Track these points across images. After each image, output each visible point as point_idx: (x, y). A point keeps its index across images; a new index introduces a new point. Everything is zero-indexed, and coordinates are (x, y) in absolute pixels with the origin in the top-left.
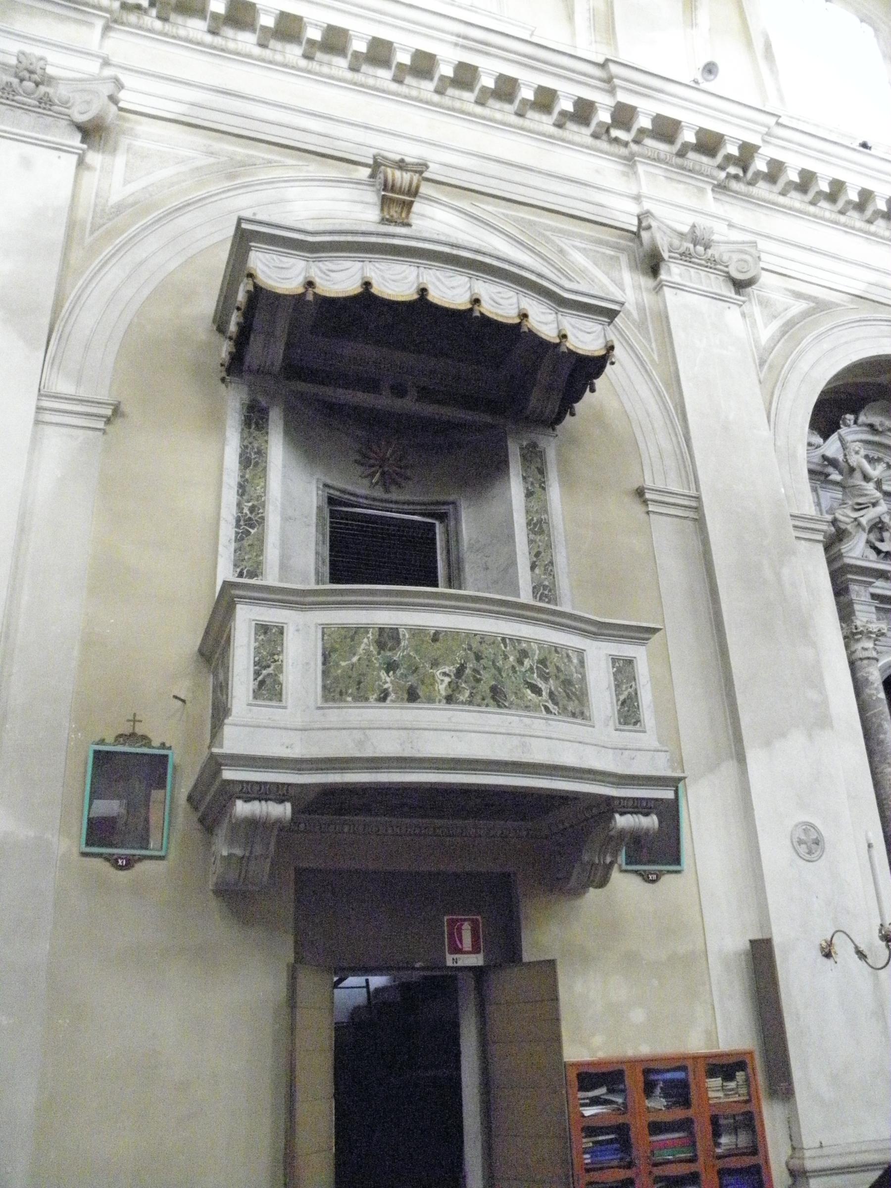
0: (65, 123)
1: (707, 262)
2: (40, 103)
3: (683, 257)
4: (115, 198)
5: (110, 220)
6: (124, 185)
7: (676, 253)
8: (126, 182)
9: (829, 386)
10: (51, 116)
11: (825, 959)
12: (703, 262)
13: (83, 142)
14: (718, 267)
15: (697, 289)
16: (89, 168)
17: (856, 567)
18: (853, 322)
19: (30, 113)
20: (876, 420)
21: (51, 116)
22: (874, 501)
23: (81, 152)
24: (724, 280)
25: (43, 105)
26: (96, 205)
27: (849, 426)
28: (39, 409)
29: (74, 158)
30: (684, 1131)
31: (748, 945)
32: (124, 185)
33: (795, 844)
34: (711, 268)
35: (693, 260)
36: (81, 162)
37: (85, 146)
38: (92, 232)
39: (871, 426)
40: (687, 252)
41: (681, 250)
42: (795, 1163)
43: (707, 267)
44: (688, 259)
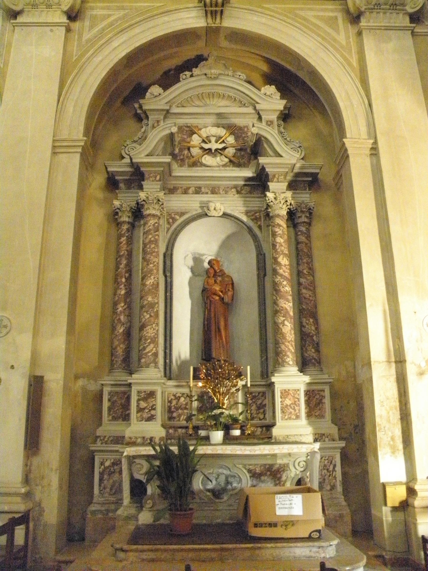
23: (66, 24)
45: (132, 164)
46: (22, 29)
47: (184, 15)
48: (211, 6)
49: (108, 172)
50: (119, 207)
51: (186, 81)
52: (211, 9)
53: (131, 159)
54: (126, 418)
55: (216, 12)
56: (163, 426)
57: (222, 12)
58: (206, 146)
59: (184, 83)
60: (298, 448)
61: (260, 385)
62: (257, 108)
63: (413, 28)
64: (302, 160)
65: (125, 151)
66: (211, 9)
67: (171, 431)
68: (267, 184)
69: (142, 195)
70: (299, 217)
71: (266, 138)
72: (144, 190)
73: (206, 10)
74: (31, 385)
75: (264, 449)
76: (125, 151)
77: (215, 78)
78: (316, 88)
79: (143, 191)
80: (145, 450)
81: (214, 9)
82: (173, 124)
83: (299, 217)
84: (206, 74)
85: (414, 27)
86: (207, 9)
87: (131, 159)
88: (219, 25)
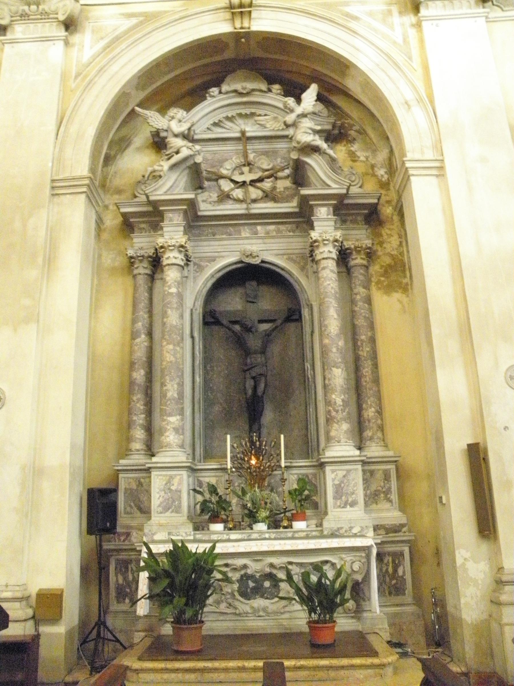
1: (41, 16)
3: (23, 18)
7: (16, 16)
12: (39, 17)
14: (51, 16)
15: (30, 38)
16: (73, 45)
17: (164, 201)
18: (172, 22)
20: (238, 86)
22: (175, 150)
23: (64, 38)
24: (57, 25)
27: (213, 97)
28: (53, 188)
29: (62, 43)
31: (466, 447)
34: (45, 19)
35: (31, 17)
36: (67, 43)
37: (67, 33)
39: (235, 91)
40: (24, 13)
41: (20, 12)
43: (41, 19)
44: (27, 18)
45: (150, 203)
46: (476, 21)
50: (370, 245)
53: (147, 197)
60: (327, 542)
61: (305, 466)
69: (160, 241)
74: (484, 459)
75: (262, 545)
77: (248, 94)
80: (234, 546)
83: (137, 268)
87: (147, 197)
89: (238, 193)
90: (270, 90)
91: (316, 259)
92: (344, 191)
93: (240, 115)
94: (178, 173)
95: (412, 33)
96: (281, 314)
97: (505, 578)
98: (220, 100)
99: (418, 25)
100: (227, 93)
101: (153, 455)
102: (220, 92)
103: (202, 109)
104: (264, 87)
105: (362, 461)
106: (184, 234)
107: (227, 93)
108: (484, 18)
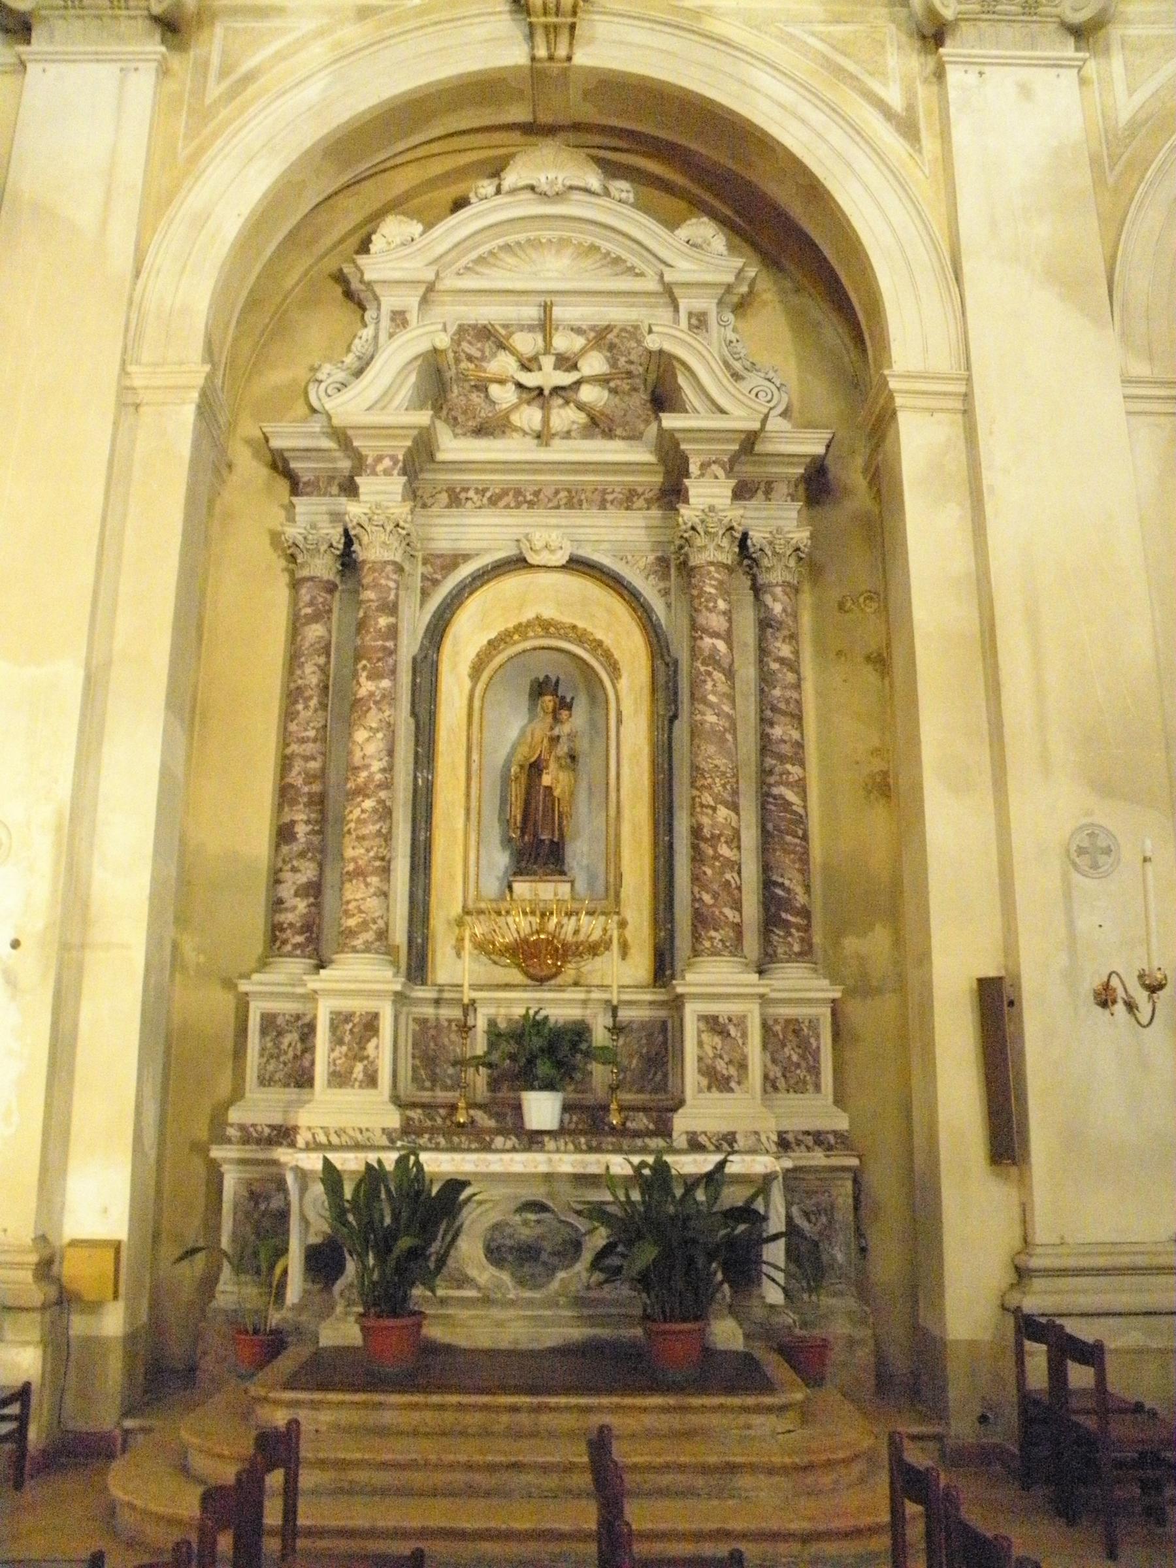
0: (1052, 27)
2: (1024, 8)
4: (1124, 117)
5: (1126, 146)
6: (1130, 95)
8: (1131, 91)
9: (778, 149)
10: (1035, 22)
11: (1100, 1009)
13: (1077, 49)
19: (1015, 25)
20: (542, 179)
21: (1035, 22)
25: (1027, 10)
26: (1106, 131)
30: (442, 1219)
31: (975, 985)
32: (1130, 95)
33: (1074, 855)
38: (1112, 169)
42: (1022, 1260)
47: (479, 31)
48: (545, 13)
49: (270, 450)
51: (486, 205)
52: (543, 19)
54: (303, 1079)
55: (556, 27)
56: (397, 1101)
57: (573, 27)
58: (530, 380)
59: (481, 208)
62: (667, 278)
63: (1080, 63)
64: (780, 419)
65: (317, 392)
66: (543, 19)
67: (416, 1114)
68: (682, 483)
70: (768, 569)
71: (684, 364)
72: (362, 497)
73: (531, 25)
76: (317, 392)
77: (558, 197)
78: (856, 290)
79: (359, 501)
81: (552, 19)
82: (440, 327)
84: (532, 188)
85: (1085, 61)
86: (533, 19)
88: (566, 65)
89: (530, 417)
90: (607, 193)
91: (692, 563)
92: (756, 426)
93: (507, 248)
94: (1120, 125)
95: (924, 93)
96: (399, 1144)
97: (1035, 1263)
98: (494, 209)
99: (939, 74)
100: (513, 191)
101: (321, 966)
102: (498, 191)
103: (641, 225)
104: (593, 180)
105: (762, 996)
106: (404, 500)
107: (513, 191)
108: (1075, 71)
